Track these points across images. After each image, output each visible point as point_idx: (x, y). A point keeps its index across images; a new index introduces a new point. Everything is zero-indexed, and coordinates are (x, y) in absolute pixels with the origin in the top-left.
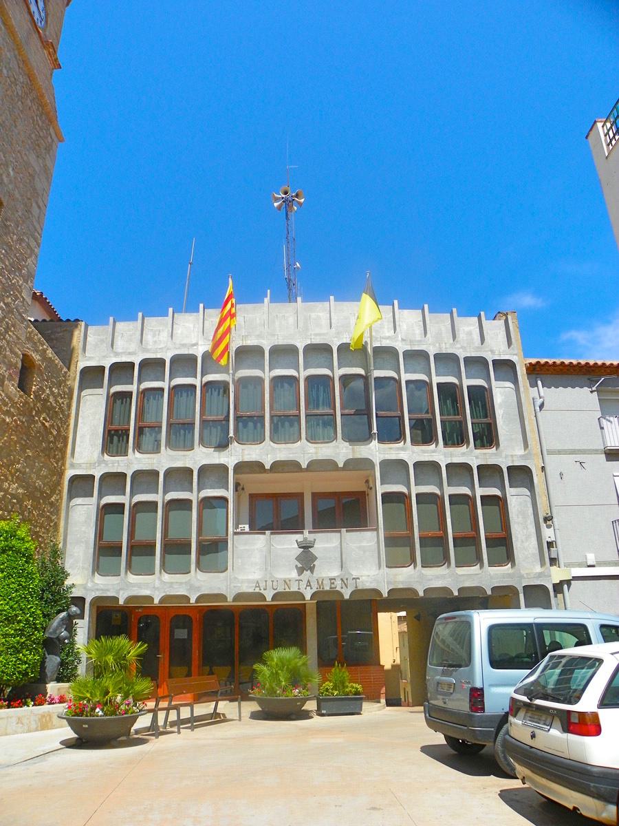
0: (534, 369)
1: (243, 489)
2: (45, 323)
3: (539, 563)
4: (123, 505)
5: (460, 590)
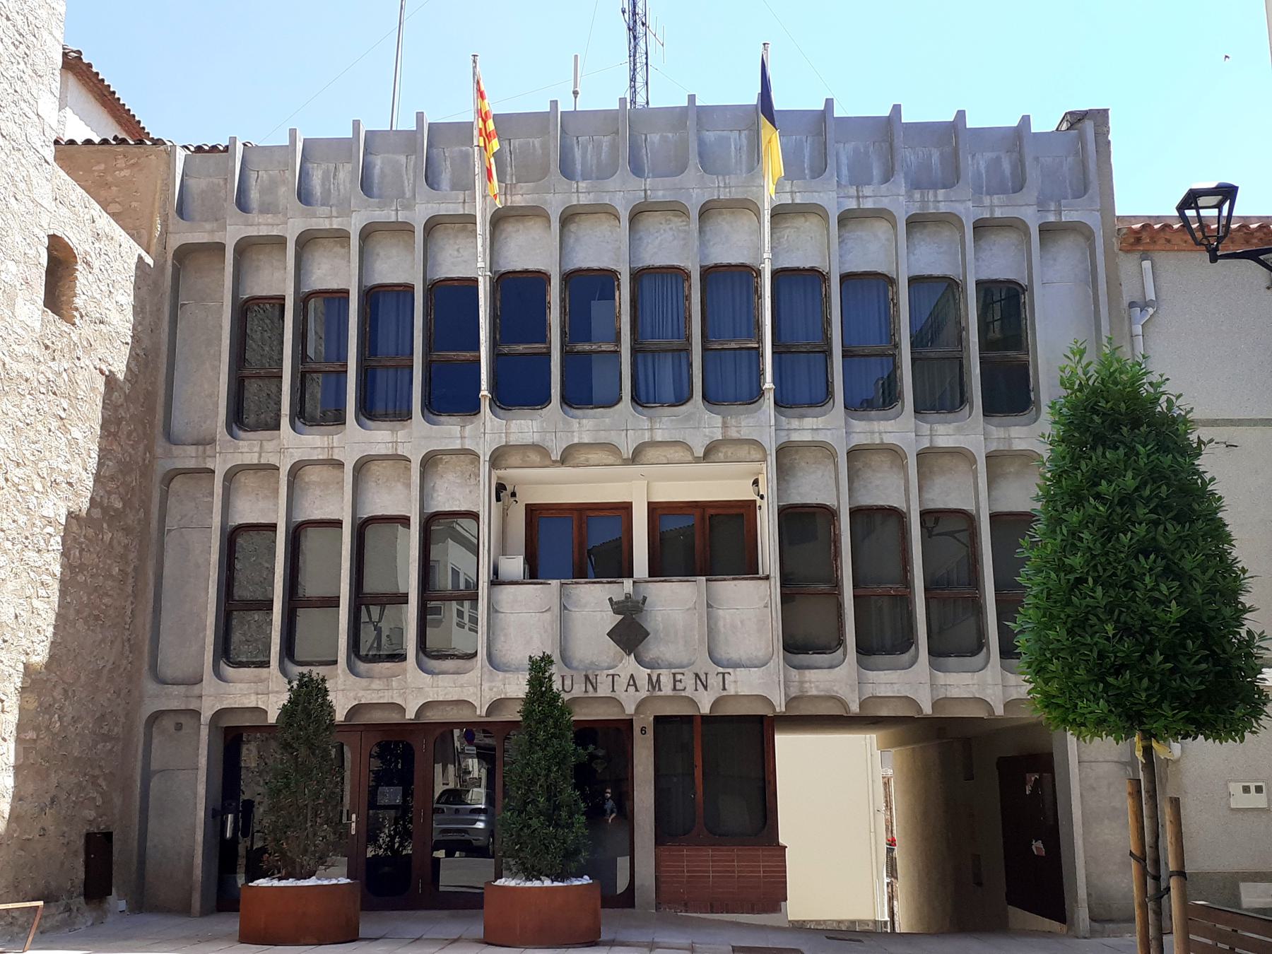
0: (1138, 240)
1: (513, 495)
2: (90, 147)
3: (946, 659)
4: (742, 513)
5: (1007, 705)
